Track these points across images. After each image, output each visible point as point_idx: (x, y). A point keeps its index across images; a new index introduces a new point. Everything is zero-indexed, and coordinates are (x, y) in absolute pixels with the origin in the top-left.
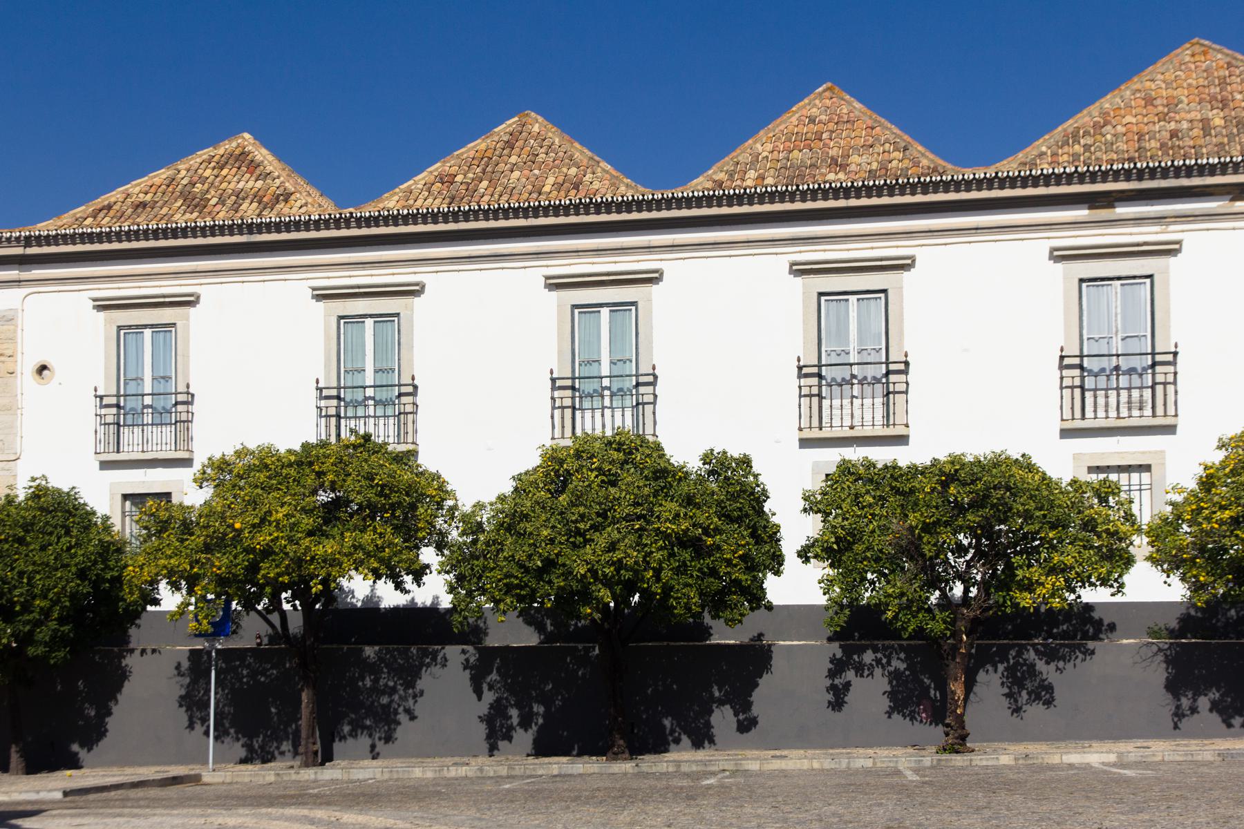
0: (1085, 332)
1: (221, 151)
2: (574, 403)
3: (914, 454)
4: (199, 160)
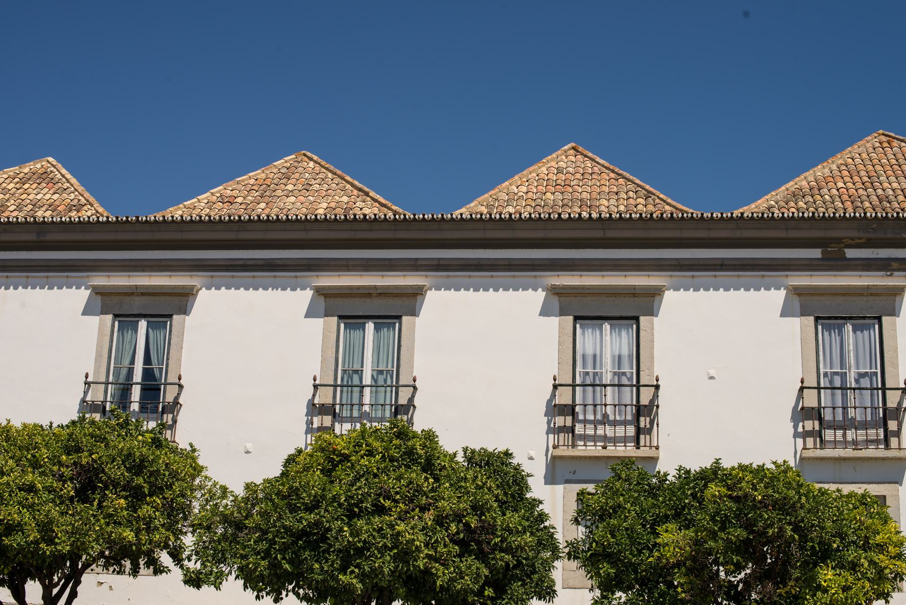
0: (821, 366)
1: (26, 170)
2: (844, 396)
3: (668, 466)
4: (5, 176)
